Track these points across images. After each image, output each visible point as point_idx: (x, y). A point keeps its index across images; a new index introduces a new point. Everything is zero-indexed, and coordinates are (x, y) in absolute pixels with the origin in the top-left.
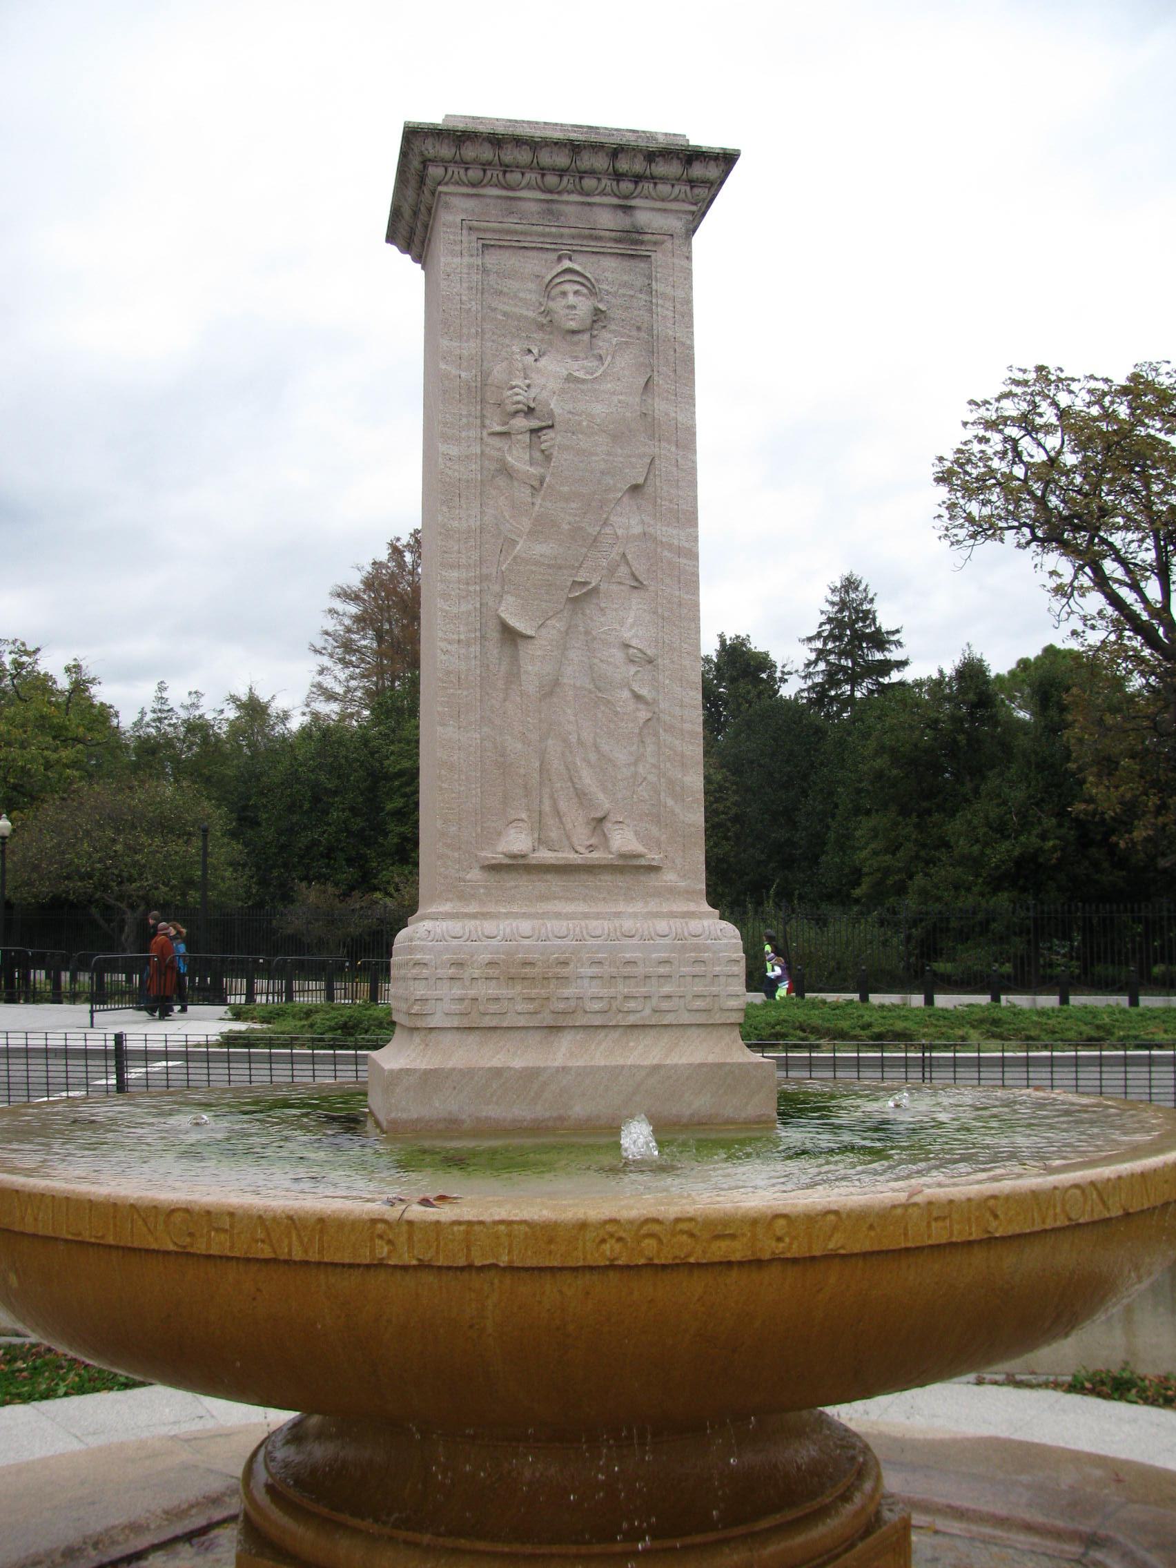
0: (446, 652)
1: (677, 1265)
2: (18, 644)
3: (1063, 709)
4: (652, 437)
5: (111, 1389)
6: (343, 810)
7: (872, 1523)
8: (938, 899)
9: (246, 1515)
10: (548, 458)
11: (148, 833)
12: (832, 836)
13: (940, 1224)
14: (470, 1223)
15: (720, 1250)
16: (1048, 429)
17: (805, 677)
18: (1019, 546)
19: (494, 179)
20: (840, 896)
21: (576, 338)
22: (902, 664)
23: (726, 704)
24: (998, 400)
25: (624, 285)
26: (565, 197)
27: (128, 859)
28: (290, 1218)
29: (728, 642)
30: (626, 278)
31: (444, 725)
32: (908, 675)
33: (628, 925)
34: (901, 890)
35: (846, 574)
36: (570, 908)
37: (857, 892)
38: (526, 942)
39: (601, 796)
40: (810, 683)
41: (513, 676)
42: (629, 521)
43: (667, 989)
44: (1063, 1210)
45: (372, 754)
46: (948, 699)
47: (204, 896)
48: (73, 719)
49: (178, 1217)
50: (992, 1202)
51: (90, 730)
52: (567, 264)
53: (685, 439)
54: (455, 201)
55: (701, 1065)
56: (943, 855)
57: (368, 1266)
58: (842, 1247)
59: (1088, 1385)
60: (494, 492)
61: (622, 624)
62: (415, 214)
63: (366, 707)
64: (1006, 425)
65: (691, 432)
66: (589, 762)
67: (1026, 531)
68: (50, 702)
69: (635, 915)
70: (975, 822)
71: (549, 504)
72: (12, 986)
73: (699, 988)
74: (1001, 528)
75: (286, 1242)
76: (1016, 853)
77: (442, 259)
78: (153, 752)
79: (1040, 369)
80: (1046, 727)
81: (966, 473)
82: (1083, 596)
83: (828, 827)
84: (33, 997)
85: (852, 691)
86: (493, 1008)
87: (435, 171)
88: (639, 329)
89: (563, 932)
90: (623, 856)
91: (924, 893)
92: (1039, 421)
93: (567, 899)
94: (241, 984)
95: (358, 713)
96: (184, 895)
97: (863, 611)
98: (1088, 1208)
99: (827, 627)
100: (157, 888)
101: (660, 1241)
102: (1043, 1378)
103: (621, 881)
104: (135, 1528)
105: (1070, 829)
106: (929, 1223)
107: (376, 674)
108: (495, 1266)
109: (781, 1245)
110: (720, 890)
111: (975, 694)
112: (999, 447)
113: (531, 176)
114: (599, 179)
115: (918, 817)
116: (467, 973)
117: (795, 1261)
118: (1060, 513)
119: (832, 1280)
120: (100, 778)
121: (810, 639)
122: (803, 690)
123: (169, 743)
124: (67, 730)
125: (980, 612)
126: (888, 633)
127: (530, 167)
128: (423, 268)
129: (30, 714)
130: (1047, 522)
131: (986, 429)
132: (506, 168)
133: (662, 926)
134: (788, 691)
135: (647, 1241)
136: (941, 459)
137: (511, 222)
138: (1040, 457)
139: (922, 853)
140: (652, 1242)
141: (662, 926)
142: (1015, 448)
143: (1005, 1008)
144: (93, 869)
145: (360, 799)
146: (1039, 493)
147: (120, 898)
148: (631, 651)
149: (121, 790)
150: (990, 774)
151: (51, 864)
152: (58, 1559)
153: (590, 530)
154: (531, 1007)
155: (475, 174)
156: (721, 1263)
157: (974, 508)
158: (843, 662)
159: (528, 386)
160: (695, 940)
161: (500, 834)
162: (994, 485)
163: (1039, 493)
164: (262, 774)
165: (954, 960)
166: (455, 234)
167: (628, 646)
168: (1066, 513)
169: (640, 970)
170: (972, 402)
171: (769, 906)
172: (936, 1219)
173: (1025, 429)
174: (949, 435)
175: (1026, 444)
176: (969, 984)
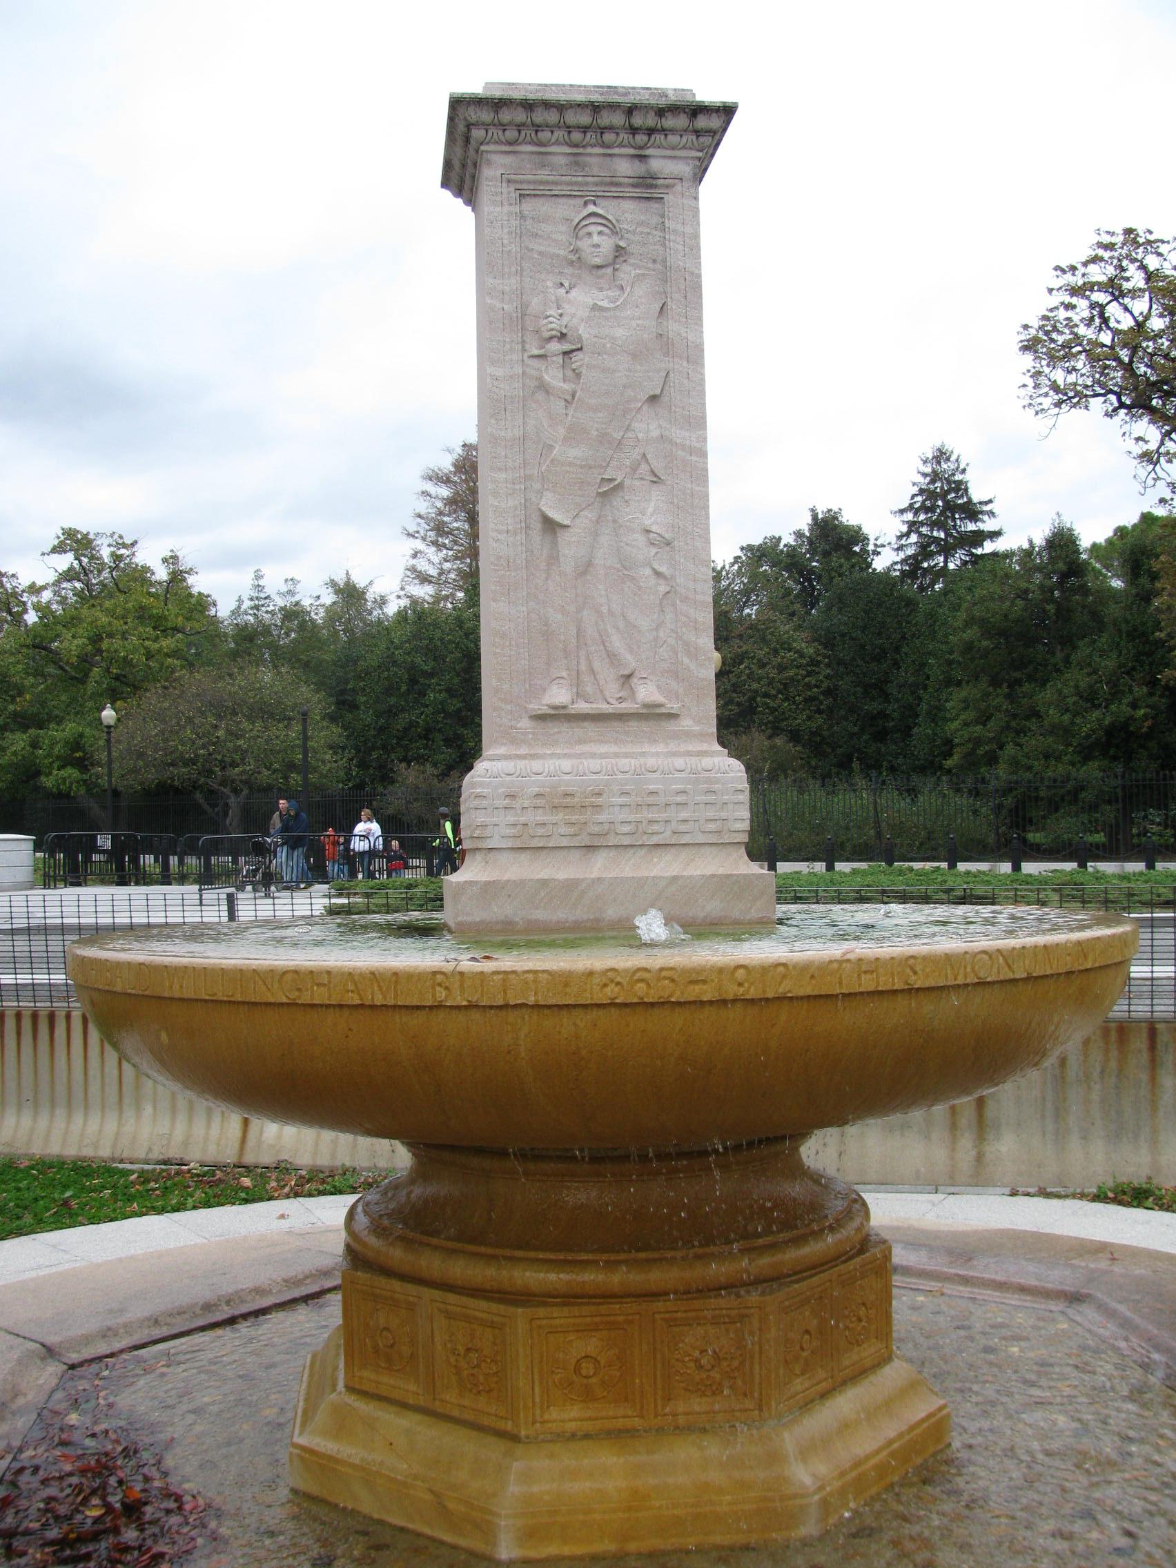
0: (497, 541)
2: (116, 537)
3: (1154, 577)
4: (667, 354)
5: (234, 1204)
6: (440, 691)
8: (1029, 768)
10: (578, 375)
11: (249, 718)
12: (924, 707)
13: (868, 976)
15: (693, 992)
16: (1135, 293)
17: (898, 549)
18: (1107, 414)
19: (528, 138)
20: (930, 767)
21: (603, 271)
22: (995, 535)
23: (819, 578)
24: (1085, 264)
25: (642, 223)
26: (589, 150)
27: (230, 745)
28: (373, 973)
29: (820, 516)
30: (643, 218)
31: (495, 600)
32: (999, 545)
33: (651, 762)
34: (992, 759)
35: (938, 445)
36: (604, 749)
37: (949, 763)
38: (567, 777)
39: (628, 657)
40: (902, 555)
41: (553, 559)
42: (648, 426)
43: (684, 815)
44: (973, 969)
45: (467, 635)
46: (1039, 569)
47: (305, 778)
48: (172, 609)
49: (289, 977)
51: (188, 619)
52: (592, 208)
53: (695, 355)
54: (494, 158)
55: (713, 876)
56: (1033, 724)
57: (431, 1007)
59: (1111, 1195)
60: (534, 406)
61: (643, 513)
62: (464, 166)
63: (461, 588)
64: (1092, 290)
65: (700, 348)
66: (618, 629)
67: (1113, 398)
68: (149, 593)
69: (657, 754)
71: (579, 415)
72: (123, 869)
74: (1086, 396)
76: (1107, 723)
77: (486, 209)
78: (250, 640)
79: (1128, 231)
80: (1137, 595)
81: (1052, 341)
82: (1170, 461)
83: (920, 699)
84: (143, 879)
85: (946, 562)
86: (541, 831)
87: (477, 134)
88: (654, 261)
90: (646, 706)
91: (1014, 763)
92: (1127, 285)
93: (602, 742)
95: (453, 595)
96: (286, 778)
97: (955, 482)
98: (995, 970)
99: (919, 499)
100: (259, 773)
101: (648, 985)
102: (1071, 1190)
103: (644, 726)
104: (259, 1291)
105: (1161, 696)
106: (859, 975)
107: (469, 556)
109: (741, 990)
110: (813, 763)
111: (1065, 563)
112: (1086, 314)
113: (560, 134)
114: (618, 134)
115: (1009, 687)
116: (518, 804)
117: (752, 1001)
118: (1148, 379)
120: (202, 665)
121: (902, 511)
122: (896, 563)
123: (266, 630)
124: (167, 620)
125: (1072, 481)
126: (980, 503)
127: (558, 126)
128: (473, 210)
129: (130, 605)
130: (1136, 388)
131: (1072, 295)
132: (538, 128)
133: (679, 762)
134: (880, 564)
135: (639, 985)
136: (1026, 327)
137: (543, 174)
138: (1127, 323)
139: (1013, 724)
141: (679, 762)
142: (1102, 314)
143: (1090, 874)
144: (196, 755)
145: (456, 681)
146: (1126, 360)
147: (223, 783)
148: (652, 535)
150: (1081, 643)
151: (156, 751)
152: (198, 1311)
153: (615, 435)
154: (571, 830)
155: (511, 134)
156: (695, 1002)
157: (1059, 376)
158: (935, 534)
159: (561, 315)
160: (707, 774)
161: (544, 690)
162: (1080, 352)
163: (1126, 360)
165: (1044, 829)
166: (495, 186)
167: (648, 531)
168: (1153, 379)
169: (662, 799)
170: (1057, 268)
172: (865, 972)
173: (1112, 294)
174: (1034, 302)
175: (1113, 310)
176: (1058, 852)
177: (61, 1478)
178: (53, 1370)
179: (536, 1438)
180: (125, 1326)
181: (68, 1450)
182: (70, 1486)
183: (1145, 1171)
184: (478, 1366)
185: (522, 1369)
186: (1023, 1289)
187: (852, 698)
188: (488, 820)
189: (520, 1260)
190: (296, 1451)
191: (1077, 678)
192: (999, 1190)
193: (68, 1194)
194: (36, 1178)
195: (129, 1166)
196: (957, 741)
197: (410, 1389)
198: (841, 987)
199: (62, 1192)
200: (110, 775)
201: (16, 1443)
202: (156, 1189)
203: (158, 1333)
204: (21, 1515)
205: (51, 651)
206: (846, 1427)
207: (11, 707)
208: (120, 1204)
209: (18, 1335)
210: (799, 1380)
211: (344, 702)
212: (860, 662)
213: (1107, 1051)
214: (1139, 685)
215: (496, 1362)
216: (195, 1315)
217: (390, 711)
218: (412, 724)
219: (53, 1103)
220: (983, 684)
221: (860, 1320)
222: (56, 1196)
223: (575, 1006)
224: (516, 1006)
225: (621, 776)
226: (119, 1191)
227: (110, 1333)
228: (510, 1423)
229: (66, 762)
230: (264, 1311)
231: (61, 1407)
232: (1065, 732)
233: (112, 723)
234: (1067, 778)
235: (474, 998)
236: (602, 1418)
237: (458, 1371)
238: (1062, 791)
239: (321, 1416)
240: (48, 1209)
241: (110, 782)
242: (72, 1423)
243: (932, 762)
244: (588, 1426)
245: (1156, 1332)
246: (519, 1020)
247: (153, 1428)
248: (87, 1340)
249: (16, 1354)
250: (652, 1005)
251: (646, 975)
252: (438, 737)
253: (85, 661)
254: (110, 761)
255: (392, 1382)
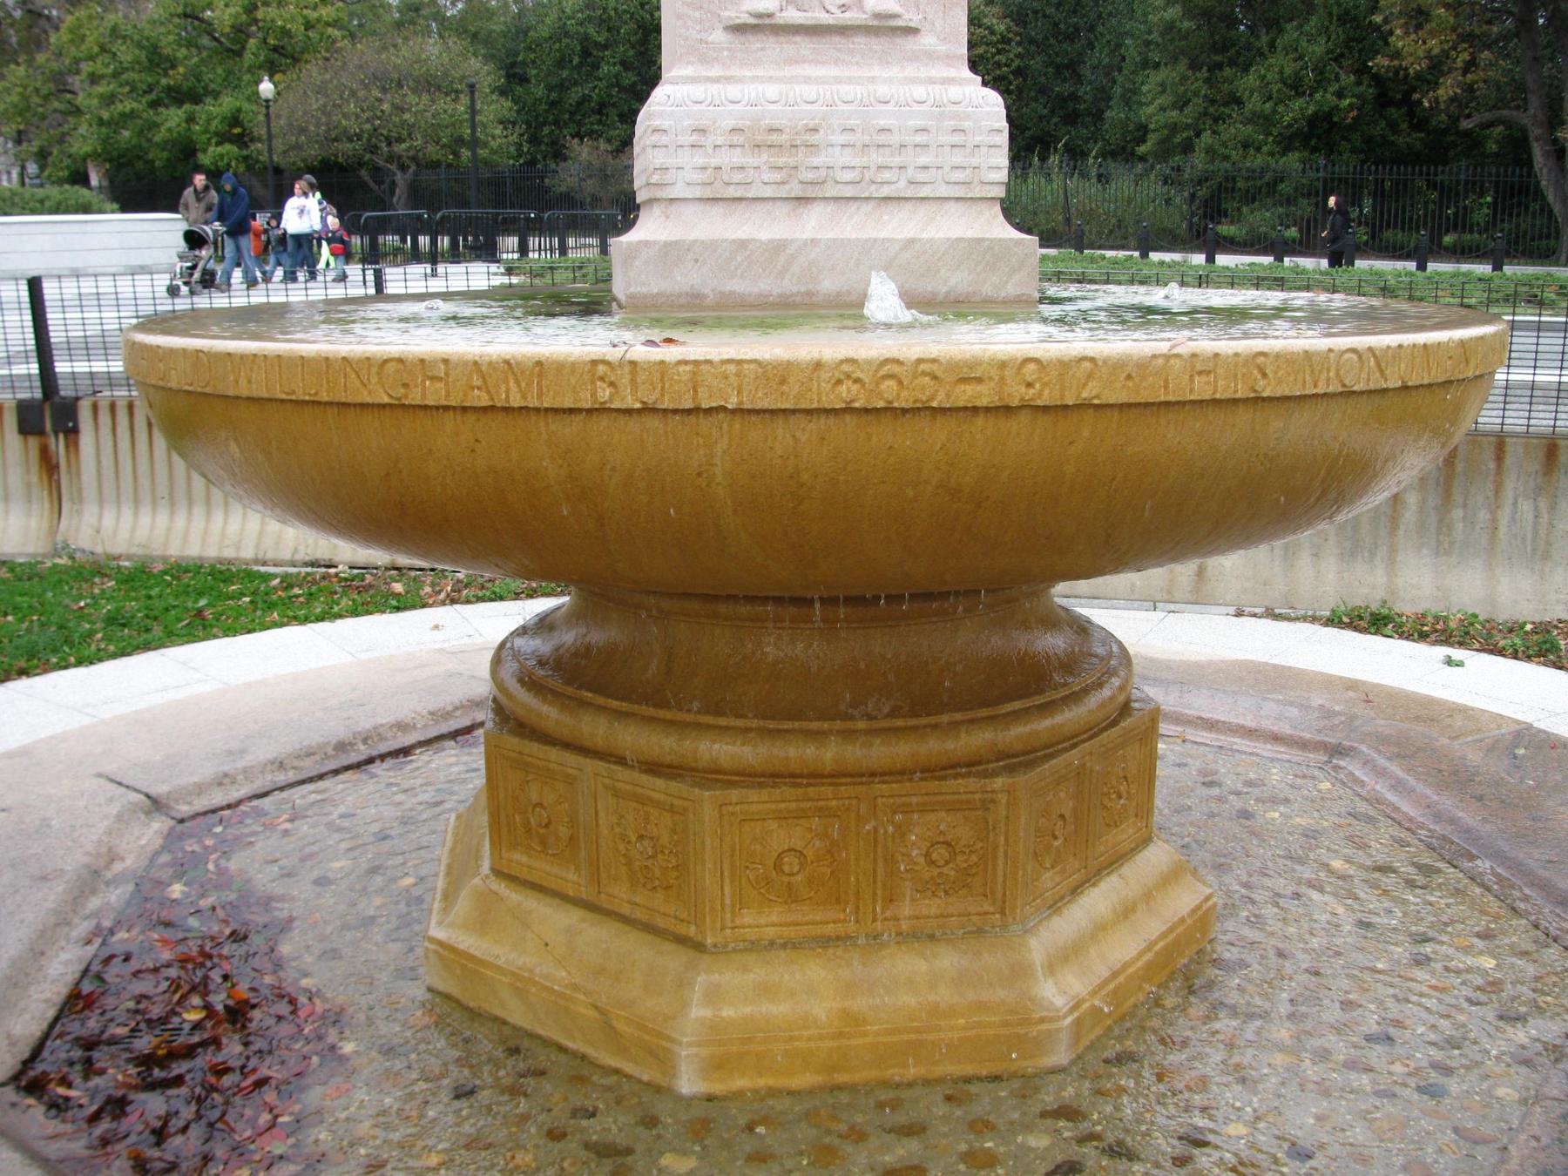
1: (919, 409)
7: (1125, 709)
8: (1226, 158)
9: (495, 700)
11: (415, 90)
12: (1118, 90)
13: (1204, 378)
14: (696, 363)
15: (966, 395)
20: (1123, 153)
28: (507, 362)
33: (883, 90)
34: (1188, 147)
36: (821, 71)
37: (1142, 149)
38: (772, 107)
43: (924, 159)
44: (1337, 374)
47: (474, 154)
49: (391, 367)
50: (1261, 360)
55: (959, 240)
57: (590, 411)
58: (1097, 397)
59: (1346, 620)
69: (890, 81)
70: (1269, 77)
73: (958, 158)
75: (503, 388)
86: (737, 177)
89: (813, 97)
90: (877, 16)
91: (1210, 151)
94: (512, 241)
101: (900, 382)
103: (876, 44)
104: (402, 727)
105: (1370, 86)
108: (724, 409)
109: (1031, 391)
116: (709, 141)
119: (1086, 433)
133: (919, 92)
139: (1211, 110)
140: (892, 383)
141: (919, 92)
145: (631, 53)
149: (385, 48)
150: (1288, 27)
152: (330, 751)
154: (778, 177)
156: (965, 408)
160: (955, 108)
164: (529, 29)
169: (895, 139)
171: (1054, 160)
172: (1200, 373)
176: (1252, 245)
177: (156, 970)
178: (159, 825)
179: (725, 946)
180: (245, 771)
181: (170, 934)
182: (167, 979)
183: (1380, 594)
184: (653, 857)
185: (709, 865)
186: (1276, 738)
187: (1043, 79)
188: (670, 162)
189: (709, 727)
190: (433, 947)
191: (1280, 64)
192: (1223, 609)
193: (202, 603)
194: (169, 585)
195: (272, 570)
196: (1152, 126)
197: (570, 878)
198: (1167, 393)
199: (196, 601)
200: (270, 150)
201: (107, 923)
202: (298, 596)
203: (282, 778)
204: (108, 1016)
205: (202, 20)
206: (1099, 930)
207: (164, 81)
208: (259, 613)
209: (120, 784)
210: (1048, 875)
211: (514, 76)
212: (1052, 41)
213: (365, 320)
214: (1347, 73)
215: (676, 855)
216: (327, 756)
217: (562, 85)
218: (586, 99)
219: (190, 502)
220: (1182, 67)
221: (1120, 797)
222: (190, 605)
223: (794, 411)
224: (710, 411)
225: (843, 107)
226: (258, 599)
227: (226, 780)
228: (693, 928)
229: (223, 138)
230: (406, 751)
231: (165, 874)
232: (1265, 121)
233: (270, 96)
234: (1263, 171)
235: (650, 400)
236: (807, 924)
237: (629, 863)
238: (1259, 183)
239: (463, 906)
240: (180, 620)
241: (271, 157)
242: (175, 896)
243: (1124, 149)
244: (790, 933)
245: (1435, 798)
246: (714, 430)
247: (267, 902)
248: (200, 789)
249: (114, 809)
250: (904, 411)
251: (897, 369)
252: (613, 112)
253: (240, 32)
254: (270, 136)
255: (548, 868)
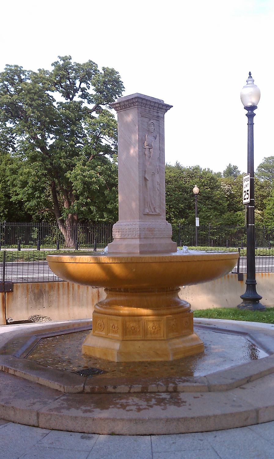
26: (152, 110)
